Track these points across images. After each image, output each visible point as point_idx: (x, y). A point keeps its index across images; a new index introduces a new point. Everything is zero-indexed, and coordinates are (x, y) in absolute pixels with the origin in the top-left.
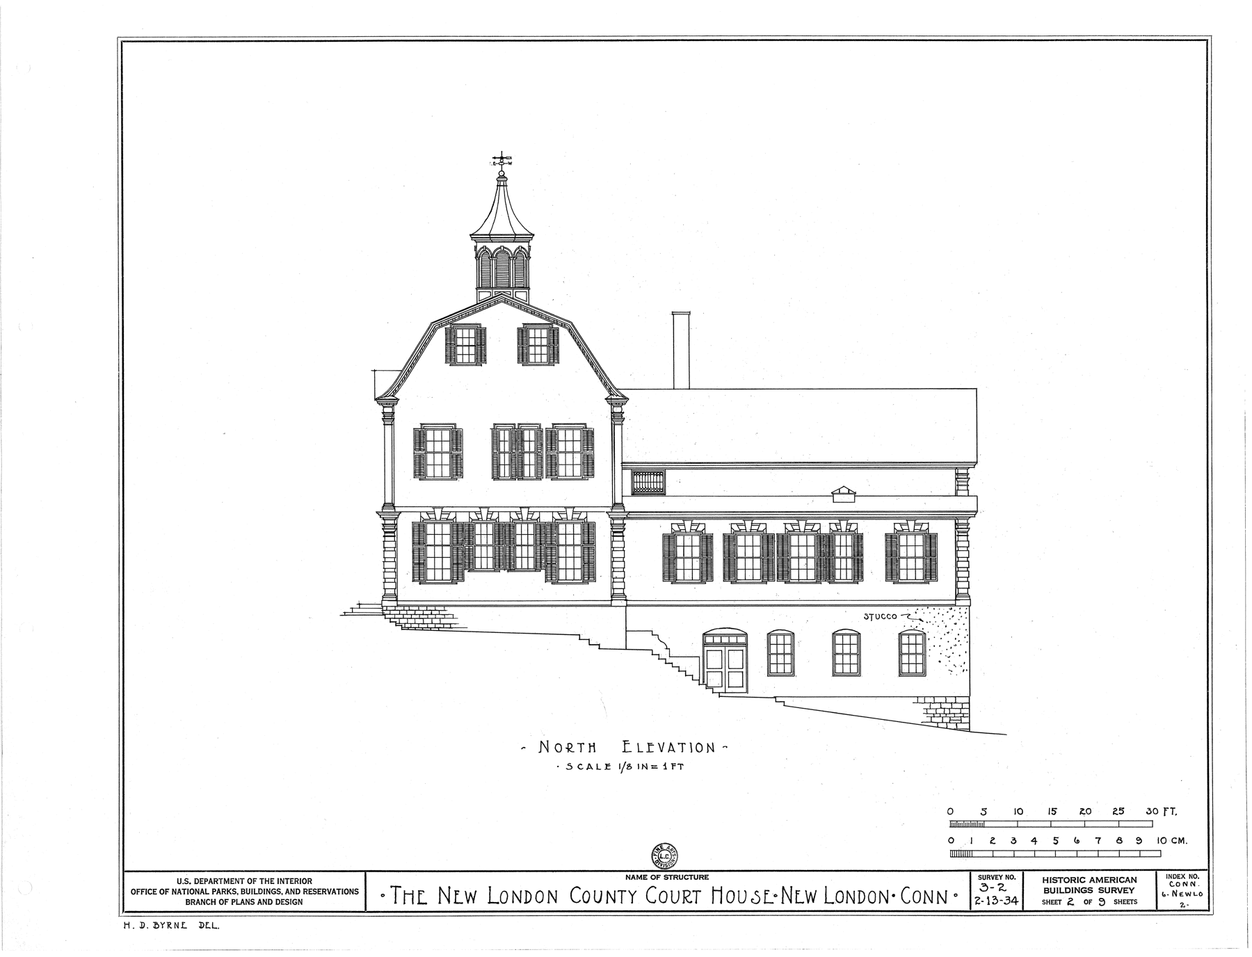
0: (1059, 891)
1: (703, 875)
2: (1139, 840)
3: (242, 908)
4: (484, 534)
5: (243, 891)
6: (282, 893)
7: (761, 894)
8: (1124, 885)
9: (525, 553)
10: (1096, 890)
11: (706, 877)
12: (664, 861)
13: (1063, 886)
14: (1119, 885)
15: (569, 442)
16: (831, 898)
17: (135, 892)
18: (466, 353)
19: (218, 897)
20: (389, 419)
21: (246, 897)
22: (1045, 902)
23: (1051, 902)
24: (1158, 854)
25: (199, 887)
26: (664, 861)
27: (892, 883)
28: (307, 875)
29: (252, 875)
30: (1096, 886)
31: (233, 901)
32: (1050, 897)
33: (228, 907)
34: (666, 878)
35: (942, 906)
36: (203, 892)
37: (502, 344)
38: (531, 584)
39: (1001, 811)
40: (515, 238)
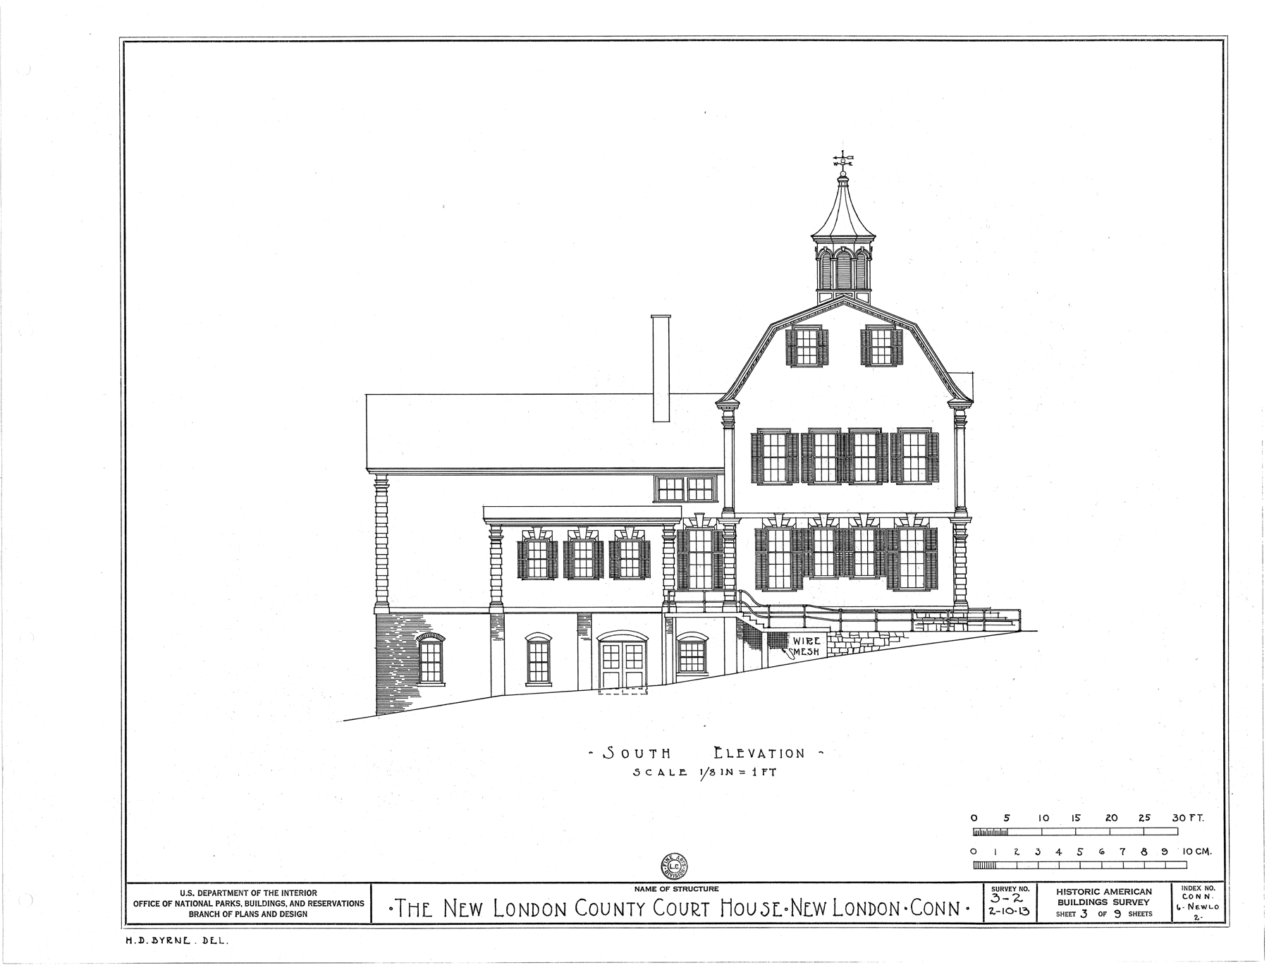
0: (1073, 903)
1: (713, 886)
2: (1165, 851)
3: (246, 920)
4: (824, 541)
5: (247, 903)
6: (288, 905)
7: (771, 906)
8: (1139, 897)
9: (865, 561)
10: (1110, 902)
11: (716, 889)
12: (674, 871)
13: (1077, 897)
14: (1134, 897)
15: (914, 446)
16: (501, 911)
17: (138, 904)
18: (807, 353)
19: (221, 909)
20: (729, 424)
21: (250, 909)
22: (1059, 914)
23: (1065, 914)
24: (1184, 865)
25: (203, 898)
26: (674, 871)
27: (902, 895)
28: (312, 887)
29: (256, 887)
30: (1110, 898)
31: (237, 913)
32: (1064, 908)
33: (232, 919)
34: (675, 889)
35: (954, 918)
36: (207, 904)
37: (845, 345)
38: (874, 592)
39: (1024, 817)
40: (856, 239)
